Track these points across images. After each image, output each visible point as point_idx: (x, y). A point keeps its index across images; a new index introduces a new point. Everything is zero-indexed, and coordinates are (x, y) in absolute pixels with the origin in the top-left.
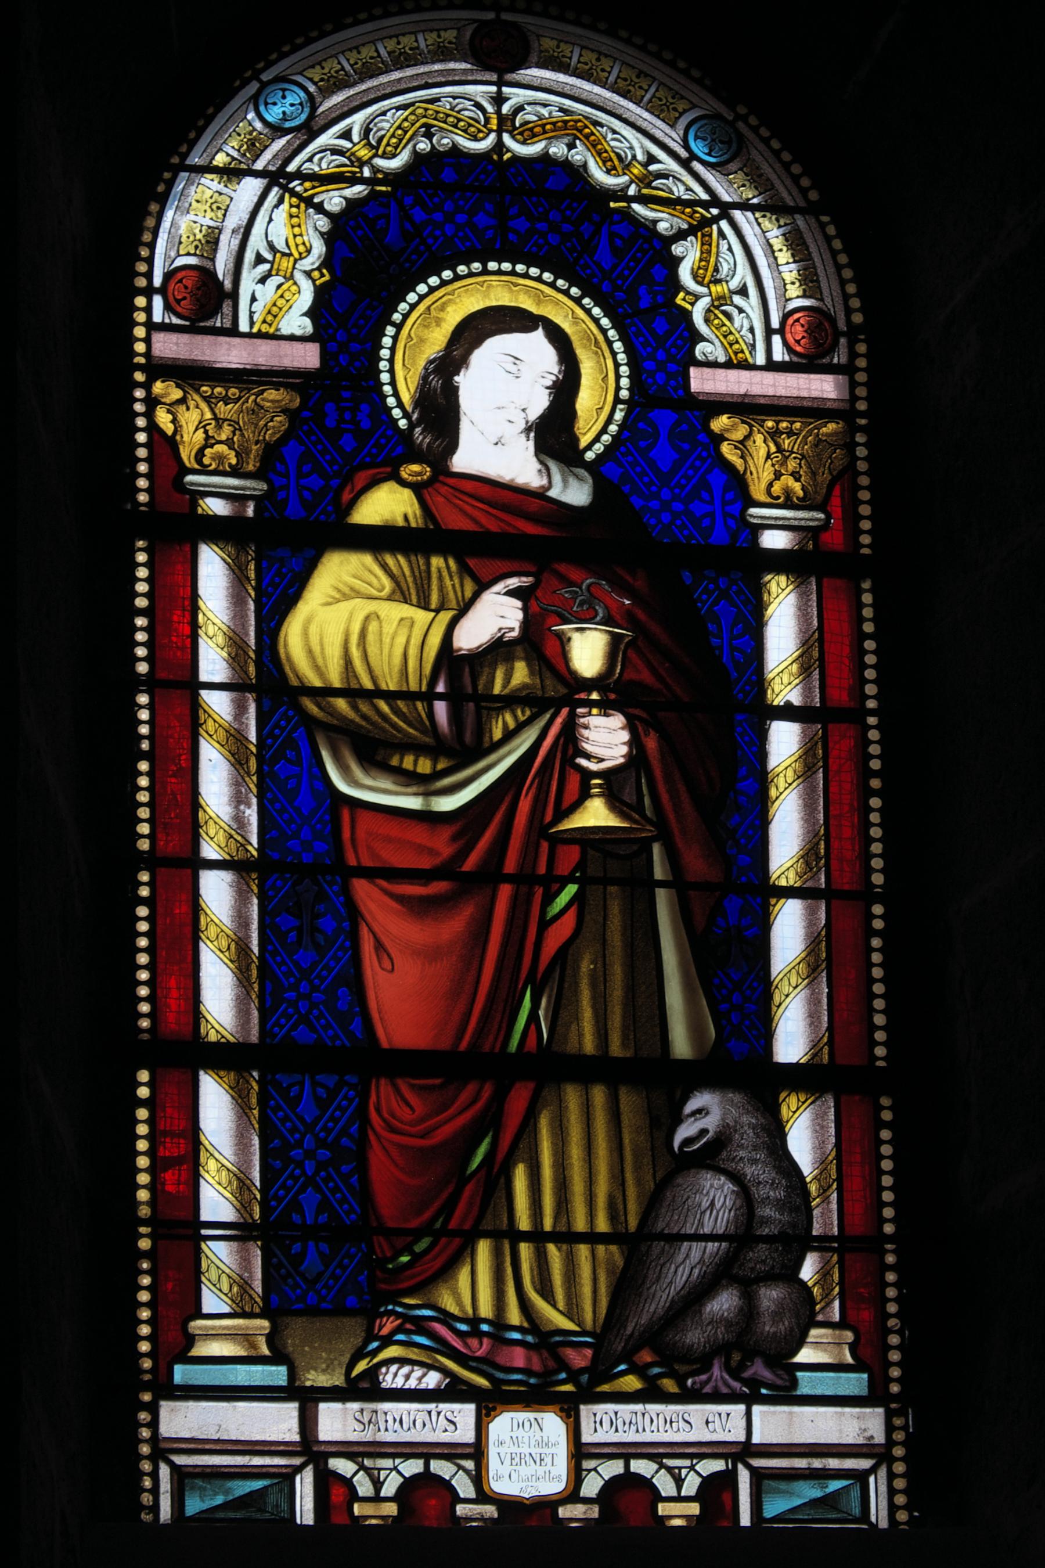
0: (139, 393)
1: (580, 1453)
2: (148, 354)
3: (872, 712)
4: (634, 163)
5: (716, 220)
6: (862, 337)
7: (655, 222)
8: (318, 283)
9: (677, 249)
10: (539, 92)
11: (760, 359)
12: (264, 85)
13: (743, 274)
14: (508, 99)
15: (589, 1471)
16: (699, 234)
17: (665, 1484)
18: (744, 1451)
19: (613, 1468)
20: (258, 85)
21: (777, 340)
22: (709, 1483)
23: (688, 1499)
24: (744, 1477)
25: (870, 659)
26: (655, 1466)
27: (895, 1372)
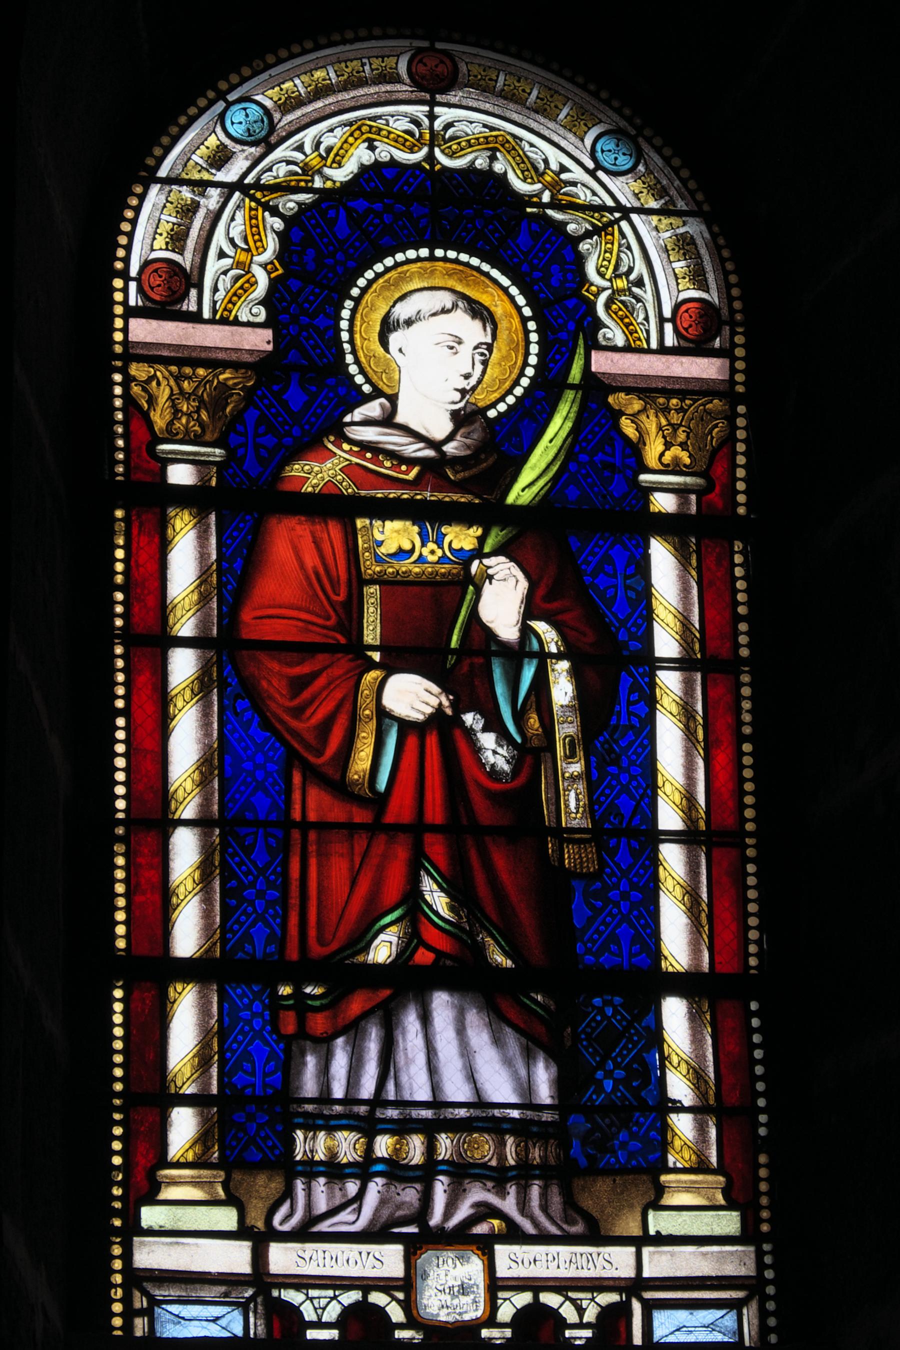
0: (118, 377)
1: (495, 1286)
2: (125, 343)
3: (750, 834)
4: (547, 171)
5: (617, 221)
6: (747, 669)
7: (565, 224)
8: (273, 275)
9: (584, 246)
10: (463, 117)
11: (654, 345)
12: (229, 104)
13: (640, 268)
14: (439, 117)
15: (505, 1299)
16: (603, 233)
17: (569, 1313)
18: (636, 1285)
19: (524, 1299)
20: (224, 105)
21: (668, 327)
22: (606, 1312)
23: (588, 1326)
24: (637, 1307)
25: (747, 760)
26: (562, 1299)
27: (765, 1214)
